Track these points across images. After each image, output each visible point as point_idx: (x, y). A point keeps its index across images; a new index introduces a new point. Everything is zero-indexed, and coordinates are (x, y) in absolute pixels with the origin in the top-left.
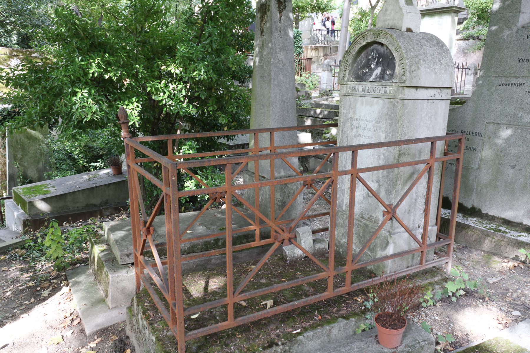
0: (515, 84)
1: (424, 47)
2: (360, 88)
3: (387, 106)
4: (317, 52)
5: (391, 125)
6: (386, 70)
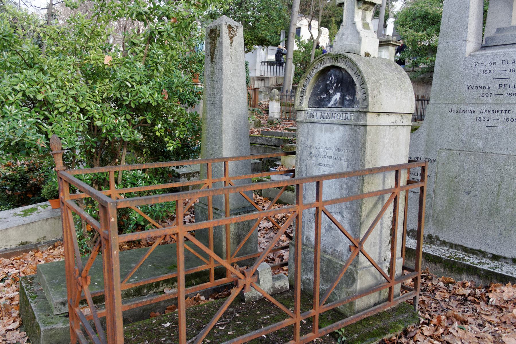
0: (465, 111)
1: (385, 72)
2: (319, 114)
3: (348, 133)
4: (263, 82)
5: (353, 152)
6: (346, 96)
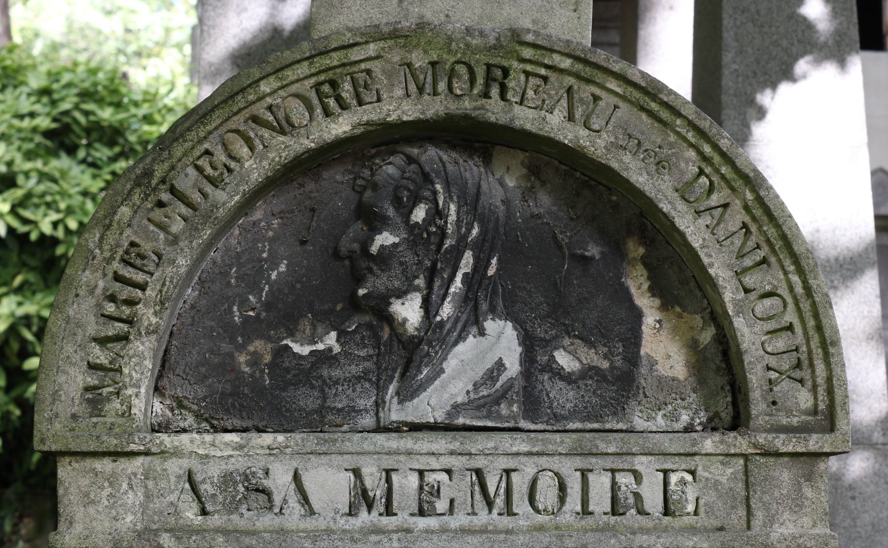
6: (550, 344)
